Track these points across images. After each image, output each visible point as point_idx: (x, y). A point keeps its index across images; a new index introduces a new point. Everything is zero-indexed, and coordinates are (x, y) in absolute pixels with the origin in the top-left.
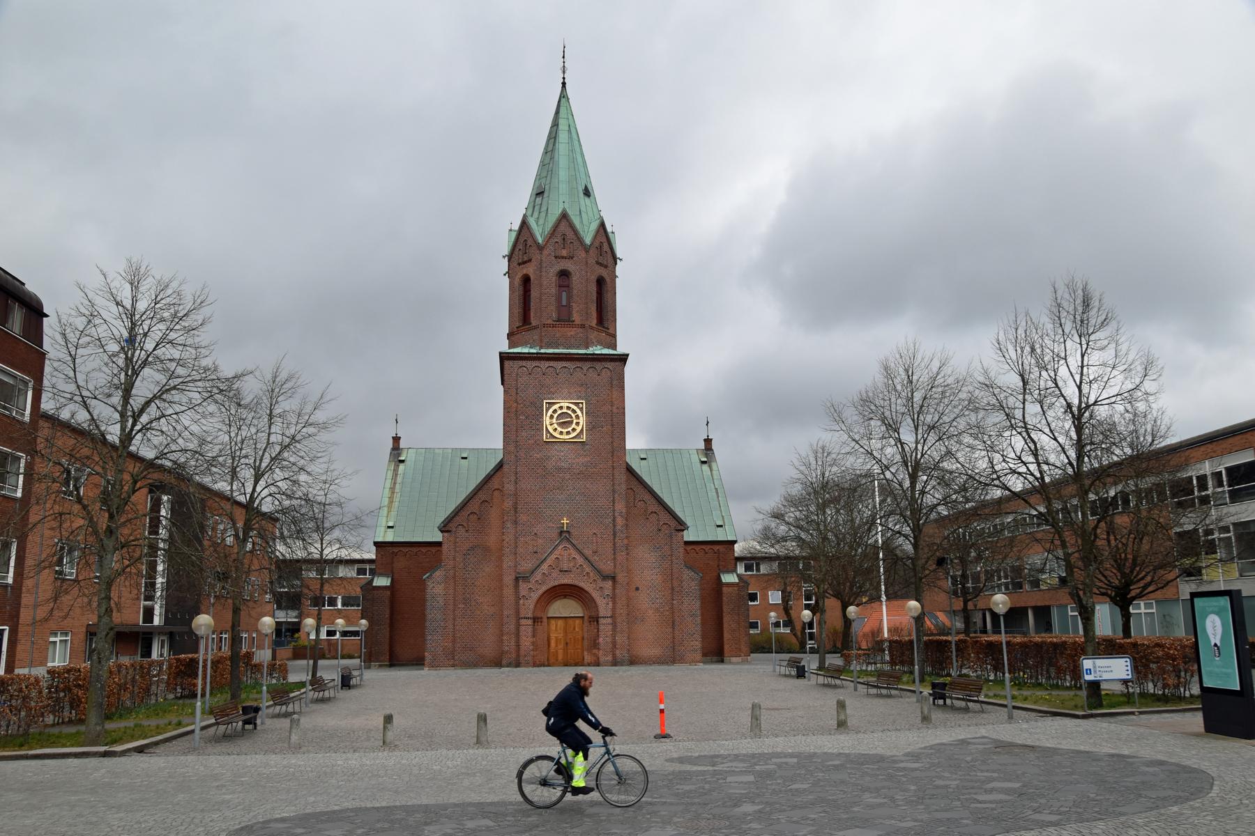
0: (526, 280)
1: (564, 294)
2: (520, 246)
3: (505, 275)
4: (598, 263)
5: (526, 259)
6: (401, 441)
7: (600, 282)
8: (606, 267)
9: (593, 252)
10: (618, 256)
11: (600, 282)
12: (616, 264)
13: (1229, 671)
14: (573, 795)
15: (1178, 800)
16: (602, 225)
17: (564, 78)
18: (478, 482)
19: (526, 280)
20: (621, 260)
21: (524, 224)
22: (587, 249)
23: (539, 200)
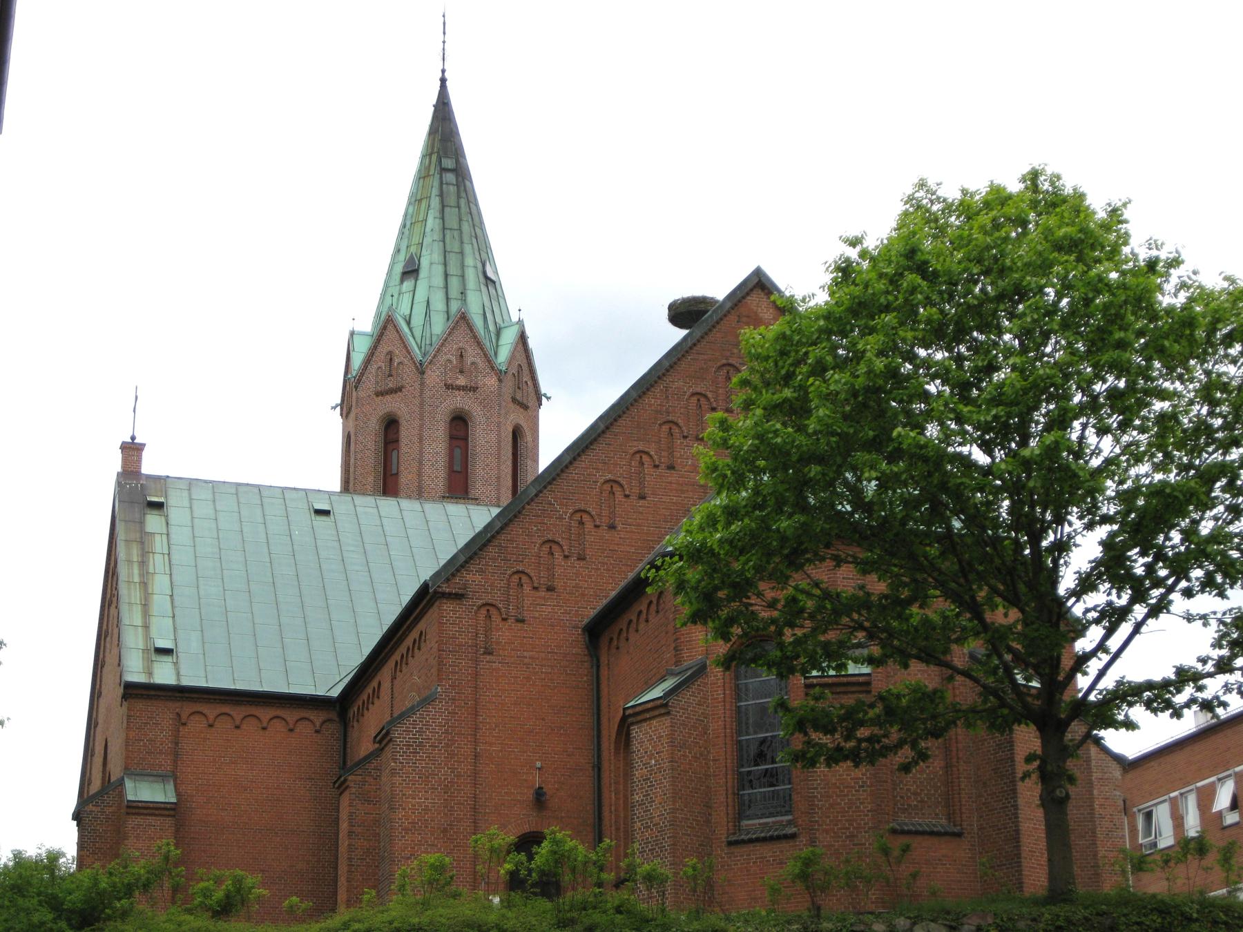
0: (391, 425)
1: (458, 452)
2: (380, 361)
3: (334, 408)
4: (514, 400)
5: (391, 385)
6: (146, 455)
7: (517, 434)
8: (526, 407)
9: (509, 383)
10: (543, 391)
11: (517, 434)
12: (540, 404)
13: (751, 730)
14: (1143, 558)
15: (1004, 598)
16: (523, 338)
17: (443, 71)
18: (385, 629)
19: (391, 425)
20: (548, 398)
21: (387, 325)
22: (500, 375)
23: (408, 285)
